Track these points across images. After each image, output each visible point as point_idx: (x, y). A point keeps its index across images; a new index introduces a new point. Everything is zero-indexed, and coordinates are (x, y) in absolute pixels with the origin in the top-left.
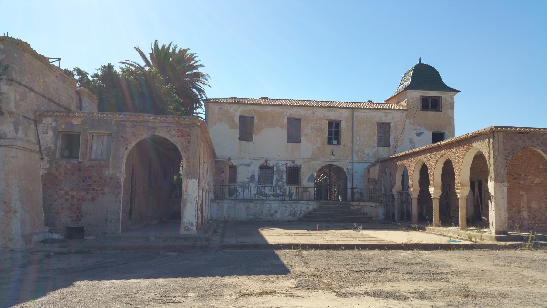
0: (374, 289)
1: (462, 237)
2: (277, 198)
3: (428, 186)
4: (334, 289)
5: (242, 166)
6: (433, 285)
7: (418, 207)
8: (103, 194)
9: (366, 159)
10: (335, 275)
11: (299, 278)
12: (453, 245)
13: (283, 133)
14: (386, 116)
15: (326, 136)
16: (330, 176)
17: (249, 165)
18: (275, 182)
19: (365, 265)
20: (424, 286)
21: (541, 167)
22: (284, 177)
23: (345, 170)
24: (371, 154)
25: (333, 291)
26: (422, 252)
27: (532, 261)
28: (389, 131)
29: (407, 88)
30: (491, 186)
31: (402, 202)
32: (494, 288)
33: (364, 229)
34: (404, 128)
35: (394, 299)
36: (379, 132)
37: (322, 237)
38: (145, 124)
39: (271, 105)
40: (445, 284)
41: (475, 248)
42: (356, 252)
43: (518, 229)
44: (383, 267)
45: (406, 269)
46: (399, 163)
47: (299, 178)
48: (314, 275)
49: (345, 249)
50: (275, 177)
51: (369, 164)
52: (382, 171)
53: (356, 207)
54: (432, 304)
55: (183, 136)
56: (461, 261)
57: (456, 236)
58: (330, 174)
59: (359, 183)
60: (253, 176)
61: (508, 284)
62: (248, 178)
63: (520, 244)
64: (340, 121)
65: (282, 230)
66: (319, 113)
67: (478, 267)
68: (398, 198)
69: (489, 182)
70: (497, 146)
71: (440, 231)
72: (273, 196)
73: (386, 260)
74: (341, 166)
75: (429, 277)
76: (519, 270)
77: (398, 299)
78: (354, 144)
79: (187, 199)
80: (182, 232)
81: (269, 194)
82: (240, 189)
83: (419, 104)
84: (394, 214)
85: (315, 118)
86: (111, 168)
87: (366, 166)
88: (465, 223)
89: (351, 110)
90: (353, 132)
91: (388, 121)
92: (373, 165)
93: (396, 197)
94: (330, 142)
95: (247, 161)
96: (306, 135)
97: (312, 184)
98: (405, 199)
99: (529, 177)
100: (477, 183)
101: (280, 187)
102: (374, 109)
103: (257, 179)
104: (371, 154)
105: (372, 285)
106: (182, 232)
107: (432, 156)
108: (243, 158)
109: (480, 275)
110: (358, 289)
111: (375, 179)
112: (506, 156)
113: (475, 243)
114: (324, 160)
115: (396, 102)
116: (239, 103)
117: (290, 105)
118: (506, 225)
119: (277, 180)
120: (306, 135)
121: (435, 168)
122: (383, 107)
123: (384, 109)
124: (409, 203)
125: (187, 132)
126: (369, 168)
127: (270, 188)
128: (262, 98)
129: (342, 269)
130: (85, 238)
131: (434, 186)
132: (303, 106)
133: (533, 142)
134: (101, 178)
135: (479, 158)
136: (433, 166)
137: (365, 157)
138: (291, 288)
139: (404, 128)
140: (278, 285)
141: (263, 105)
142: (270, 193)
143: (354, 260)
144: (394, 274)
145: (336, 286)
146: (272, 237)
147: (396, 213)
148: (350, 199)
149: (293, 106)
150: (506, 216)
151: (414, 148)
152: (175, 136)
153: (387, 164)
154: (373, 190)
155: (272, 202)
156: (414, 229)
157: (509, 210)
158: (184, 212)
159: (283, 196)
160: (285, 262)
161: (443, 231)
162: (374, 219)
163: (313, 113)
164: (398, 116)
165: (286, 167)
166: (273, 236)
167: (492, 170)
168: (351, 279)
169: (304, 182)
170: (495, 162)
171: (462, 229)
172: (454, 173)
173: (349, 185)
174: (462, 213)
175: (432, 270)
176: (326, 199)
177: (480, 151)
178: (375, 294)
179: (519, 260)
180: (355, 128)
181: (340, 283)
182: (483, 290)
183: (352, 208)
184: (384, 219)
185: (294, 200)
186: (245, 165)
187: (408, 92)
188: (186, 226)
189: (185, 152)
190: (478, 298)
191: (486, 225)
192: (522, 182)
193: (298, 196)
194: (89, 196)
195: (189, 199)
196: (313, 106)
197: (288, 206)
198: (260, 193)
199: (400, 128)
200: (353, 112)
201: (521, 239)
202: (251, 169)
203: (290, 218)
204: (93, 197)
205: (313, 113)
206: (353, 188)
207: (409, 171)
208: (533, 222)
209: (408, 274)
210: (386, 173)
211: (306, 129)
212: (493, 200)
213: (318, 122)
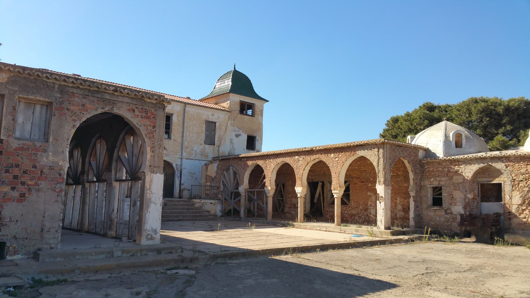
8: (38, 190)
9: (194, 156)
14: (213, 115)
23: (174, 166)
24: (198, 151)
28: (215, 130)
33: (258, 226)
38: (100, 96)
55: (148, 118)
78: (184, 139)
79: (150, 199)
80: (144, 242)
83: (238, 108)
86: (50, 154)
89: (183, 105)
91: (214, 120)
92: (211, 162)
104: (198, 151)
106: (144, 242)
111: (211, 177)
112: (391, 164)
115: (214, 102)
125: (152, 114)
130: (8, 258)
134: (35, 167)
152: (138, 116)
158: (147, 216)
180: (185, 124)
188: (148, 234)
189: (150, 138)
194: (16, 194)
195: (153, 199)
199: (224, 128)
204: (22, 195)
209: (377, 270)
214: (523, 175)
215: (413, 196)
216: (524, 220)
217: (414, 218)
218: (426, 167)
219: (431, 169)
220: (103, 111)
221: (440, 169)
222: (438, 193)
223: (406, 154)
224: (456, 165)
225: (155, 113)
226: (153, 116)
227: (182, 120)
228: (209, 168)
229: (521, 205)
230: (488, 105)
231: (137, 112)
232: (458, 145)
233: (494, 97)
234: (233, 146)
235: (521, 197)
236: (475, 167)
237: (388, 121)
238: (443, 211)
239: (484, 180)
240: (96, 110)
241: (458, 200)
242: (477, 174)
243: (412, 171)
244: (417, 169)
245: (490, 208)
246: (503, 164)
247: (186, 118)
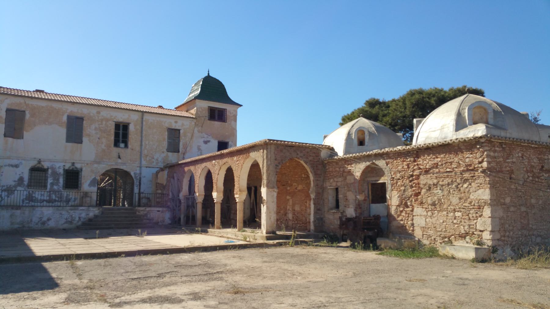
0: (151, 295)
1: (239, 238)
2: (51, 204)
3: (212, 191)
4: (108, 300)
5: (7, 168)
6: (209, 285)
7: (202, 211)
9: (155, 164)
10: (111, 285)
11: (69, 292)
12: (230, 245)
13: (62, 132)
14: (176, 122)
15: (113, 138)
16: (115, 180)
17: (17, 166)
18: (49, 186)
19: (145, 271)
20: (199, 287)
22: (61, 181)
23: (132, 174)
24: (160, 159)
25: (106, 301)
26: (202, 254)
27: (293, 256)
28: (179, 137)
29: (197, 98)
30: (264, 191)
31: (188, 207)
32: (260, 283)
33: (149, 234)
34: (192, 136)
35: (169, 303)
36: (169, 138)
37: (102, 245)
39: (48, 99)
40: (220, 282)
41: (249, 247)
42: (137, 259)
43: (284, 229)
44: (163, 271)
45: (185, 272)
46: (186, 169)
47: (80, 182)
48: (87, 287)
49: (125, 256)
50: (50, 181)
51: (158, 169)
52: (171, 176)
53: (142, 213)
54: (205, 303)
56: (236, 260)
57: (234, 237)
58: (116, 178)
59: (147, 187)
60: (21, 179)
61: (273, 278)
62: (15, 181)
63: (285, 242)
64: (129, 124)
65: (54, 239)
66: (104, 113)
67: (249, 264)
68: (184, 203)
69: (262, 188)
70: (269, 157)
71: (220, 233)
72: (47, 201)
73: (167, 265)
74: (128, 170)
75: (206, 278)
76: (282, 265)
77: (173, 303)
78: (143, 147)
81: (41, 200)
82: (3, 193)
83: (206, 114)
84: (180, 219)
85: (100, 118)
87: (155, 170)
88: (242, 225)
89: (140, 113)
90: (142, 136)
91: (177, 128)
92: (162, 170)
93: (182, 201)
94: (116, 144)
95: (15, 162)
96: (89, 135)
97: (95, 189)
98: (190, 203)
99: (294, 184)
100: (253, 188)
101: (55, 192)
102: (164, 114)
103: (26, 183)
104: (160, 159)
105: (149, 291)
107: (216, 163)
108: (9, 158)
109: (249, 272)
110: (134, 297)
111: (162, 184)
112: (277, 166)
113: (249, 243)
114: (109, 164)
115: (186, 109)
116: (7, 94)
117: (71, 102)
118: (275, 225)
119: (52, 184)
120: (89, 135)
121: (218, 174)
122: (173, 113)
123: (174, 116)
124: (194, 207)
126: (157, 173)
127: (43, 193)
128: (37, 91)
129: (120, 278)
131: (217, 191)
132: (86, 104)
133: (298, 154)
135: (255, 166)
136: (217, 172)
137: (153, 162)
138: (58, 303)
139: (192, 136)
140: (42, 302)
141: (38, 98)
142: (42, 198)
143: (134, 267)
144: (173, 278)
145: (110, 297)
146: (42, 248)
147: (182, 217)
148: (137, 204)
149: (74, 102)
150: (275, 218)
151: (201, 155)
153: (173, 169)
154: (160, 195)
155: (44, 209)
156: (197, 232)
157: (278, 213)
159: (58, 201)
160: (54, 275)
161: (223, 232)
162: (160, 224)
163: (98, 113)
164: (187, 123)
165: (64, 169)
166: (40, 246)
167: (265, 177)
168: (128, 287)
169: (86, 185)
170: (267, 171)
171: (239, 231)
172: (234, 180)
173: (136, 190)
174: (240, 216)
175: (209, 270)
176: (111, 205)
177: (255, 161)
178: (151, 300)
179: (282, 256)
180: (144, 132)
181: (115, 293)
182: (251, 286)
183: (137, 213)
184: (170, 224)
185: (72, 206)
186: (12, 166)
187: (197, 101)
190: (246, 294)
191: (259, 226)
192: (288, 188)
193: (77, 202)
196: (98, 106)
197: (64, 212)
198: (30, 198)
199: (189, 135)
200: (143, 115)
201: (288, 237)
202: (18, 171)
203: (66, 226)
205: (98, 113)
206: (140, 193)
207: (195, 177)
208: (296, 222)
209: (186, 276)
210: (174, 178)
211: (89, 129)
212: (265, 204)
213: (104, 123)
214: (400, 172)
216: (402, 222)
217: (314, 221)
219: (331, 169)
221: (338, 169)
223: (302, 155)
224: (349, 164)
227: (140, 128)
228: (160, 175)
229: (399, 206)
230: (423, 98)
232: (361, 143)
233: (429, 88)
235: (399, 197)
236: (363, 165)
239: (372, 179)
242: (366, 172)
245: (377, 209)
246: (384, 162)
247: (144, 127)
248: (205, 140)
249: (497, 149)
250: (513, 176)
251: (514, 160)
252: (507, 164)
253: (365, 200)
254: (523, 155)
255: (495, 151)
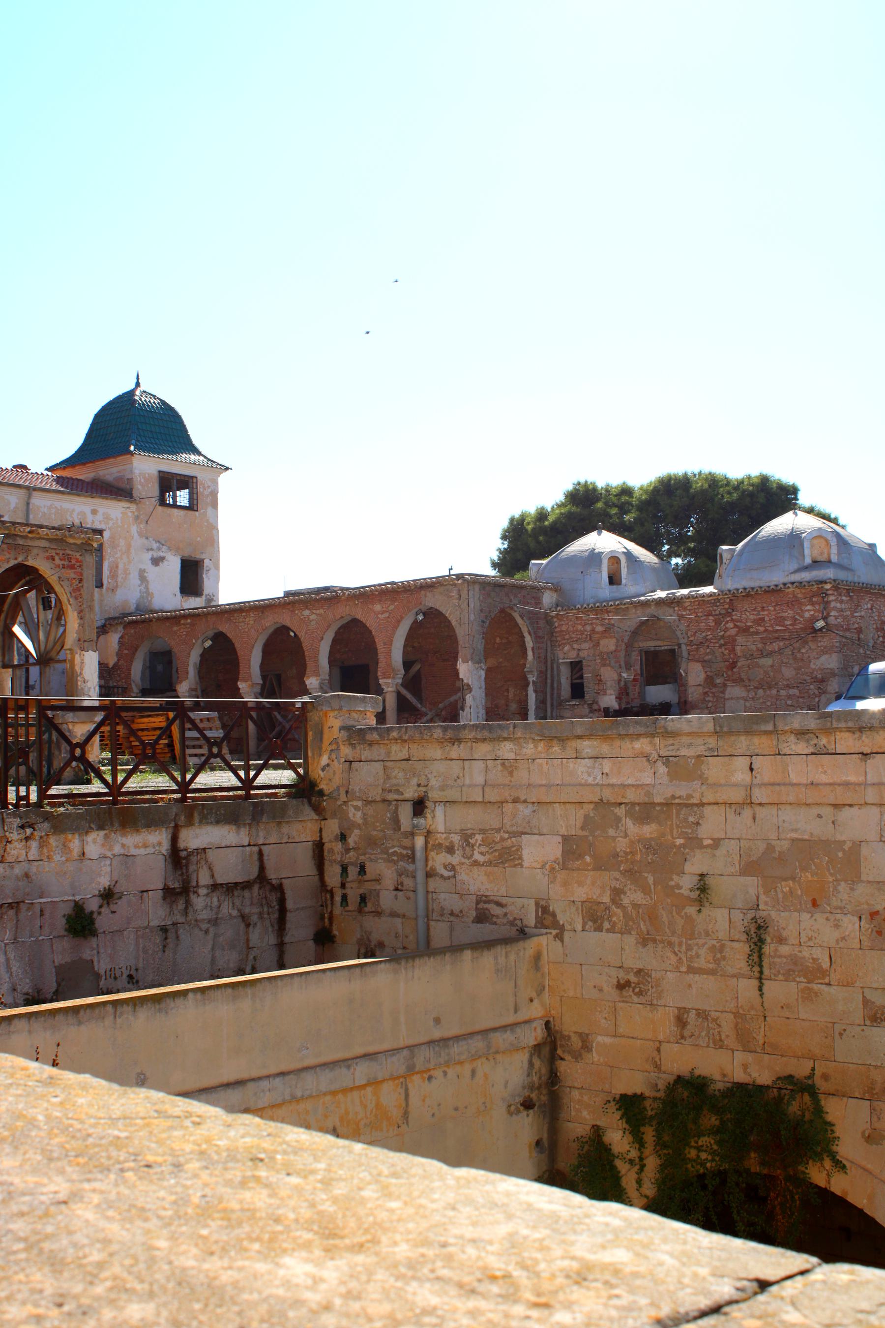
14: (94, 512)
21: (498, 640)
55: (72, 567)
70: (747, 614)
79: (82, 689)
89: (23, 492)
112: (483, 622)
125: (77, 561)
200: (29, 497)
215: (534, 682)
218: (556, 624)
219: (564, 628)
220: (16, 562)
221: (580, 627)
222: (578, 675)
225: (80, 558)
226: (78, 564)
231: (57, 561)
234: (147, 588)
237: (579, 484)
238: (586, 706)
240: (8, 562)
241: (609, 684)
243: (530, 633)
244: (539, 628)
248: (156, 554)
249: (844, 598)
250: (862, 636)
251: (863, 613)
252: (854, 619)
253: (635, 680)
254: (872, 606)
255: (841, 602)
